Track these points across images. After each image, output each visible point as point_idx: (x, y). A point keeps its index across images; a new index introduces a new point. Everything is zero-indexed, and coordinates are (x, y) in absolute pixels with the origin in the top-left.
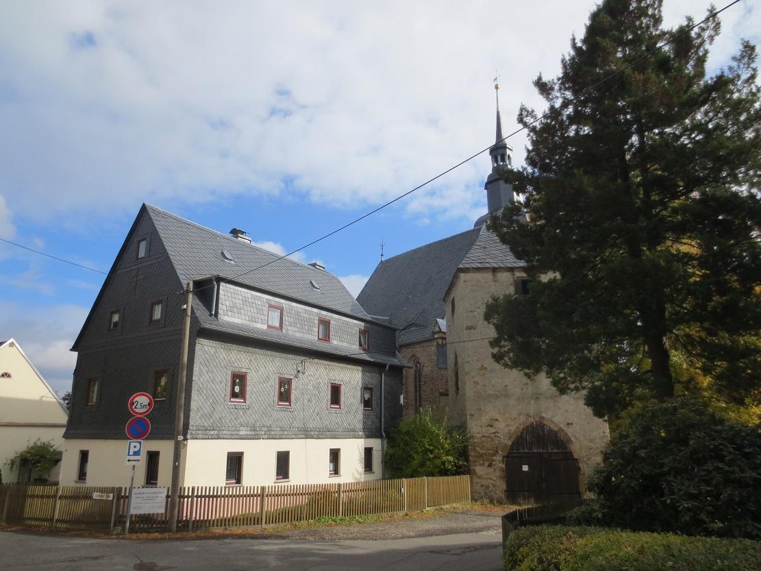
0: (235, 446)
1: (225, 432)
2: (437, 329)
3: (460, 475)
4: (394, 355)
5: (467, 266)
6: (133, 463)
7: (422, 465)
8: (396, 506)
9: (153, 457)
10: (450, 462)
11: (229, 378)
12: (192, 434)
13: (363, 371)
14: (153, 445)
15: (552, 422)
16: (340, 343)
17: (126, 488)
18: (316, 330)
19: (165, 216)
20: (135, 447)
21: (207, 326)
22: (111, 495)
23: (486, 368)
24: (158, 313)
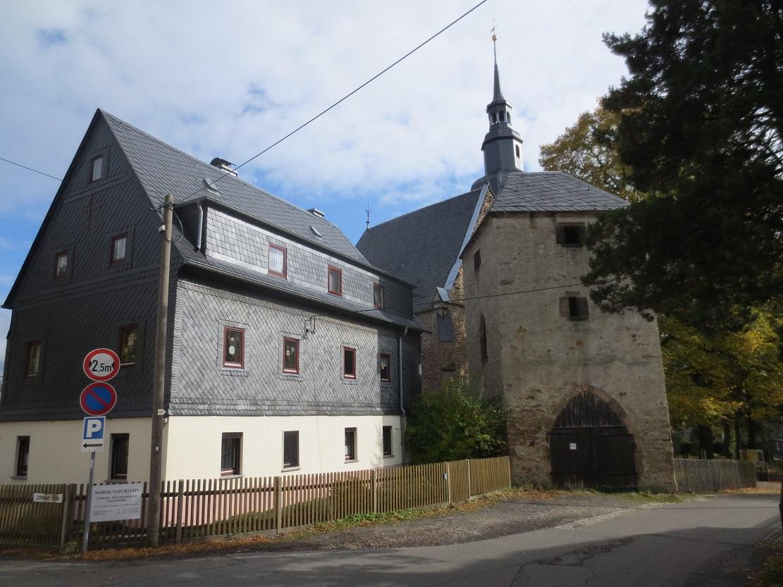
0: (233, 425)
1: (218, 407)
2: (437, 299)
3: (496, 456)
4: (411, 318)
5: (501, 210)
6: (92, 449)
7: (452, 445)
8: (437, 496)
9: (120, 443)
10: (486, 441)
11: (222, 335)
12: (174, 408)
13: (380, 335)
14: (120, 426)
15: (603, 392)
16: (354, 299)
17: (82, 486)
18: (326, 280)
19: (127, 128)
20: (94, 426)
21: (192, 262)
22: (61, 496)
23: (525, 330)
24: (121, 248)
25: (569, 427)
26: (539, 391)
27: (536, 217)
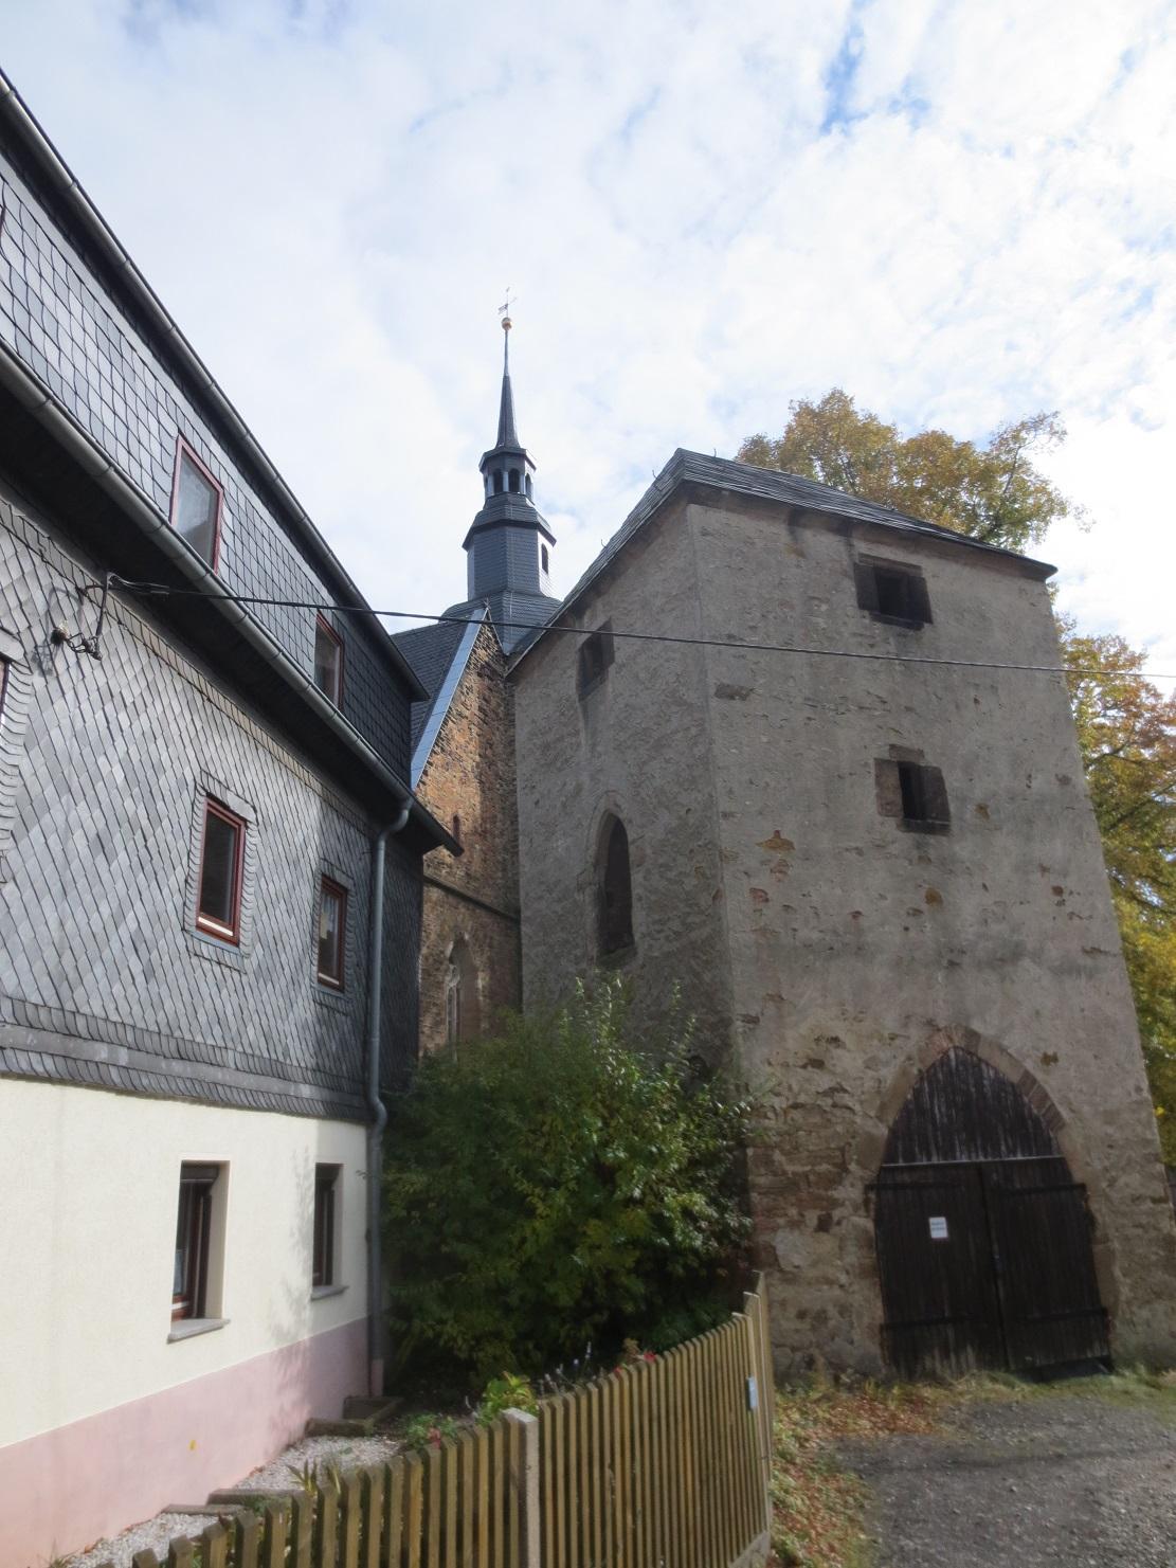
15: (1003, 1050)
23: (788, 845)
25: (925, 1163)
26: (835, 1040)
27: (805, 526)
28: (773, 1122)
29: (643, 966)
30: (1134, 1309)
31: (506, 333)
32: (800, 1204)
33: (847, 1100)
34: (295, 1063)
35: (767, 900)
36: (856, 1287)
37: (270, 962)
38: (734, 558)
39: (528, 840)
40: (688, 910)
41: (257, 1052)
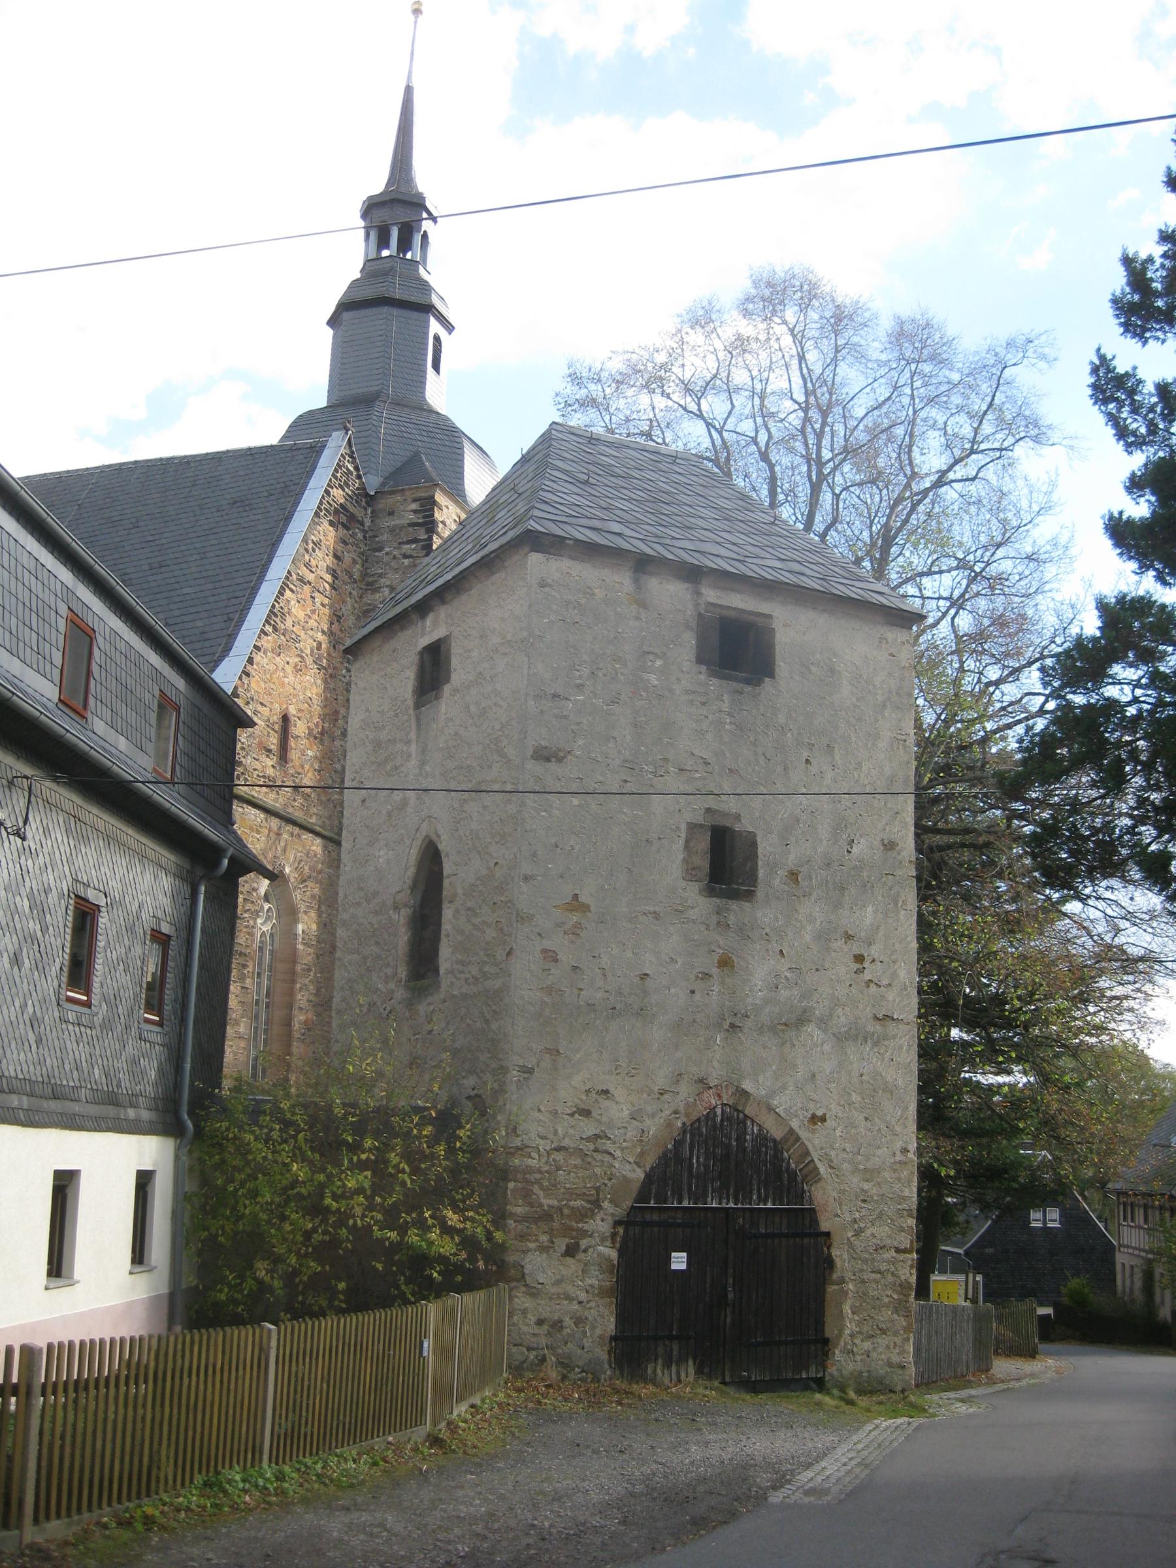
15: (770, 1109)
23: (585, 908)
28: (535, 1161)
29: (444, 1001)
30: (857, 1341)
31: (416, 22)
32: (551, 1232)
33: (609, 1145)
34: (125, 1092)
35: (556, 961)
36: (593, 1304)
37: (111, 1015)
38: (570, 611)
39: (351, 839)
40: (485, 959)
41: (100, 1087)
